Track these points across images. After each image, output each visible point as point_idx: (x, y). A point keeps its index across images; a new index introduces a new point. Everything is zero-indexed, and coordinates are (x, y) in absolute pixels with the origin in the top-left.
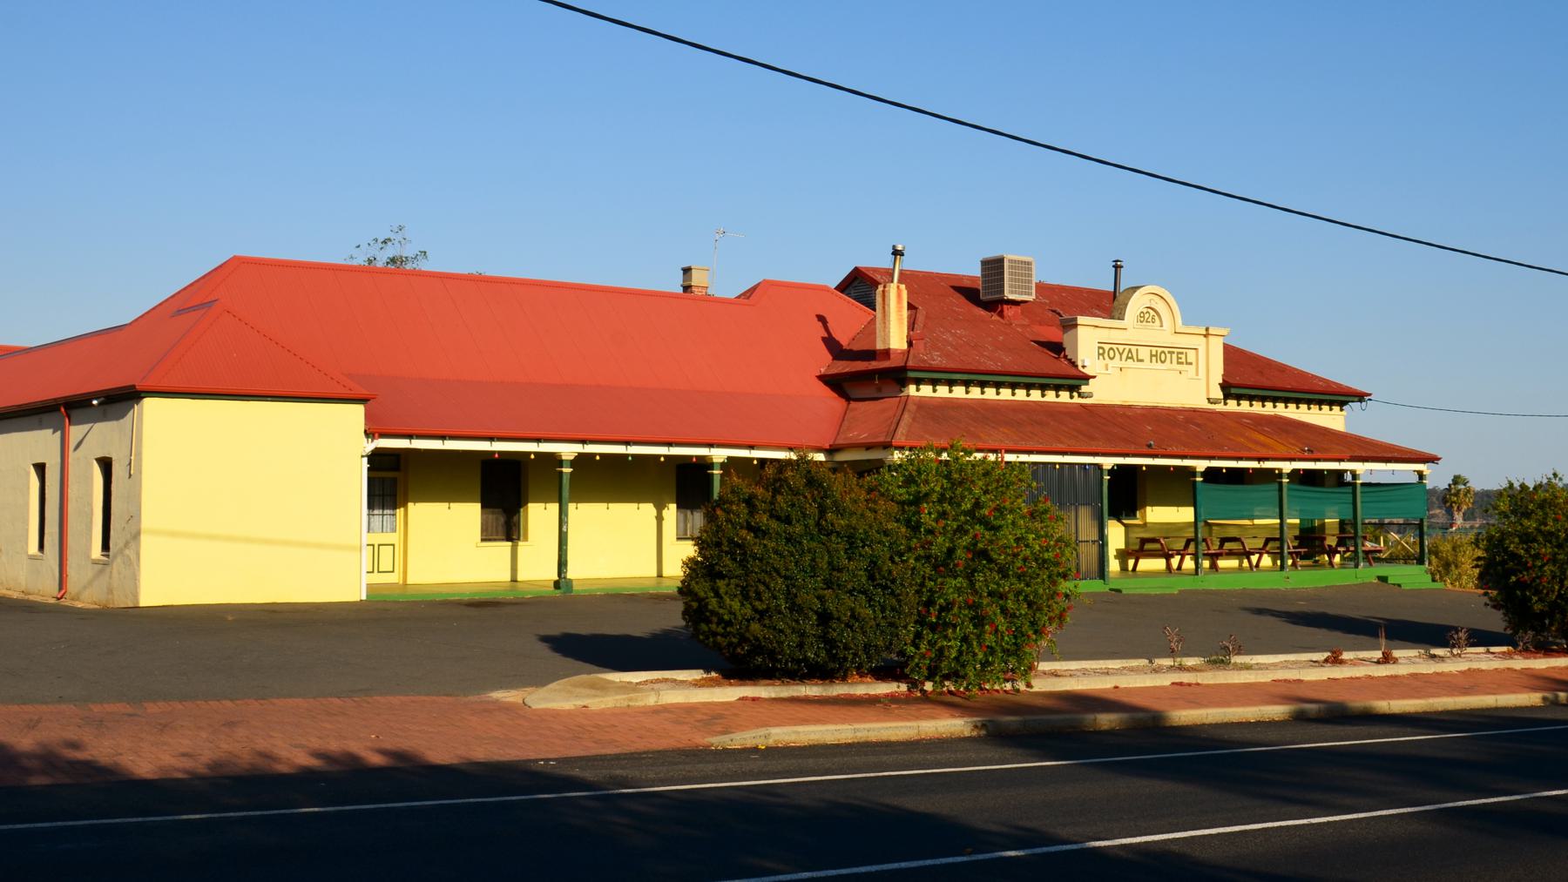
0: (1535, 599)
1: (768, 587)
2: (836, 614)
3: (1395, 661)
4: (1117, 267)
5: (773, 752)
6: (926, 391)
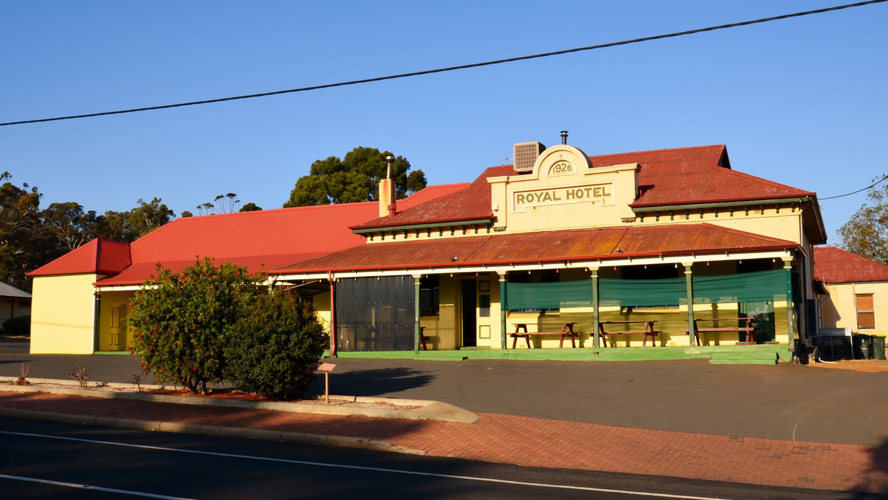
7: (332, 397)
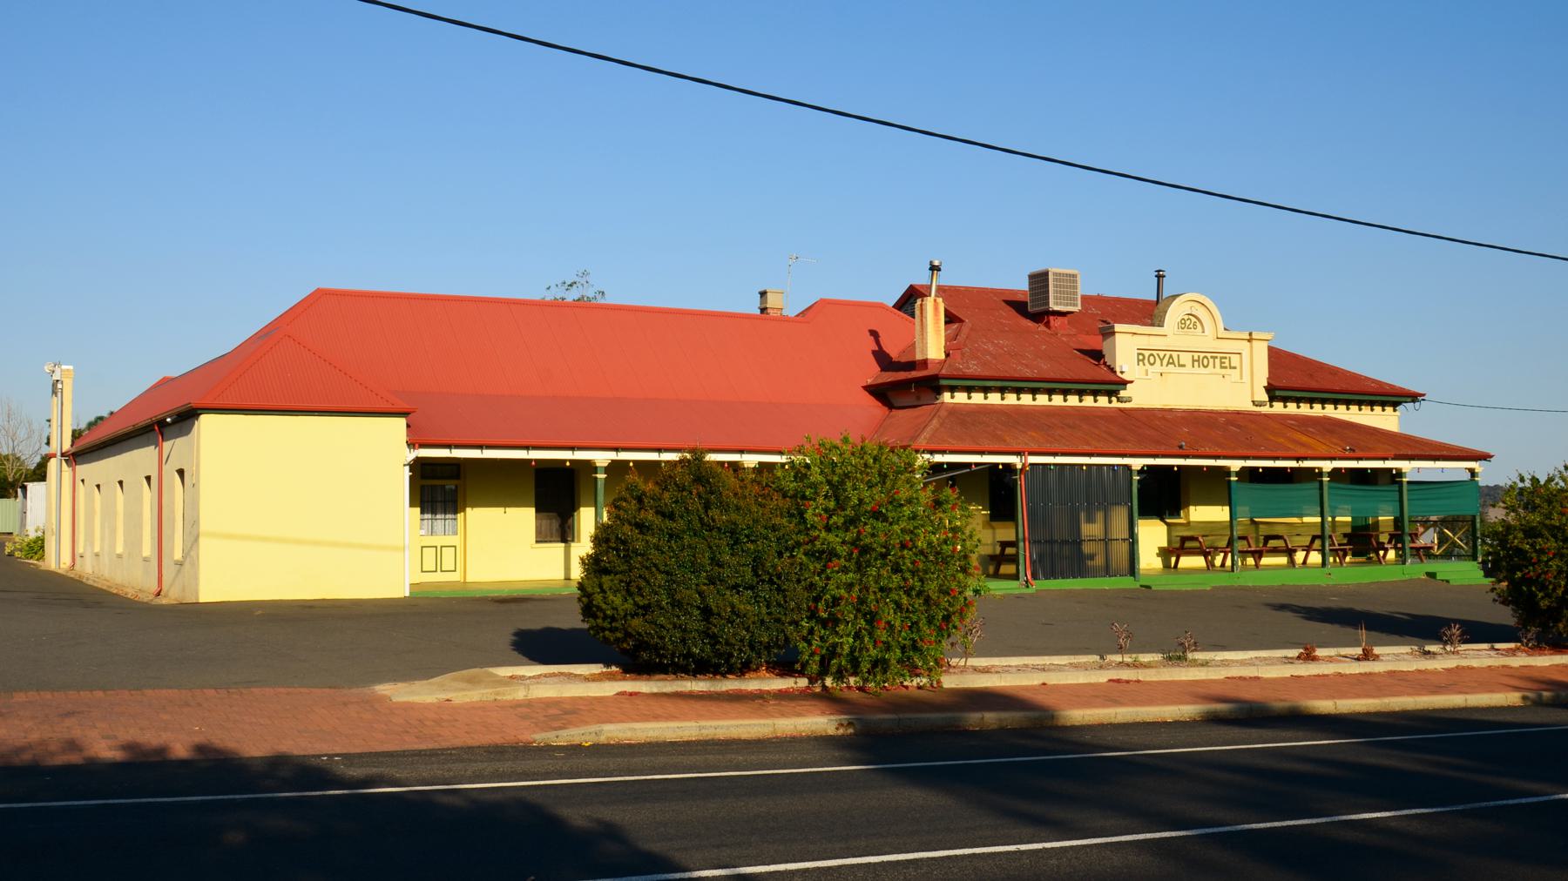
0: (1540, 595)
1: (648, 582)
2: (715, 610)
3: (1377, 658)
4: (1159, 277)
5: (599, 750)
6: (961, 398)
7: (1464, 647)
